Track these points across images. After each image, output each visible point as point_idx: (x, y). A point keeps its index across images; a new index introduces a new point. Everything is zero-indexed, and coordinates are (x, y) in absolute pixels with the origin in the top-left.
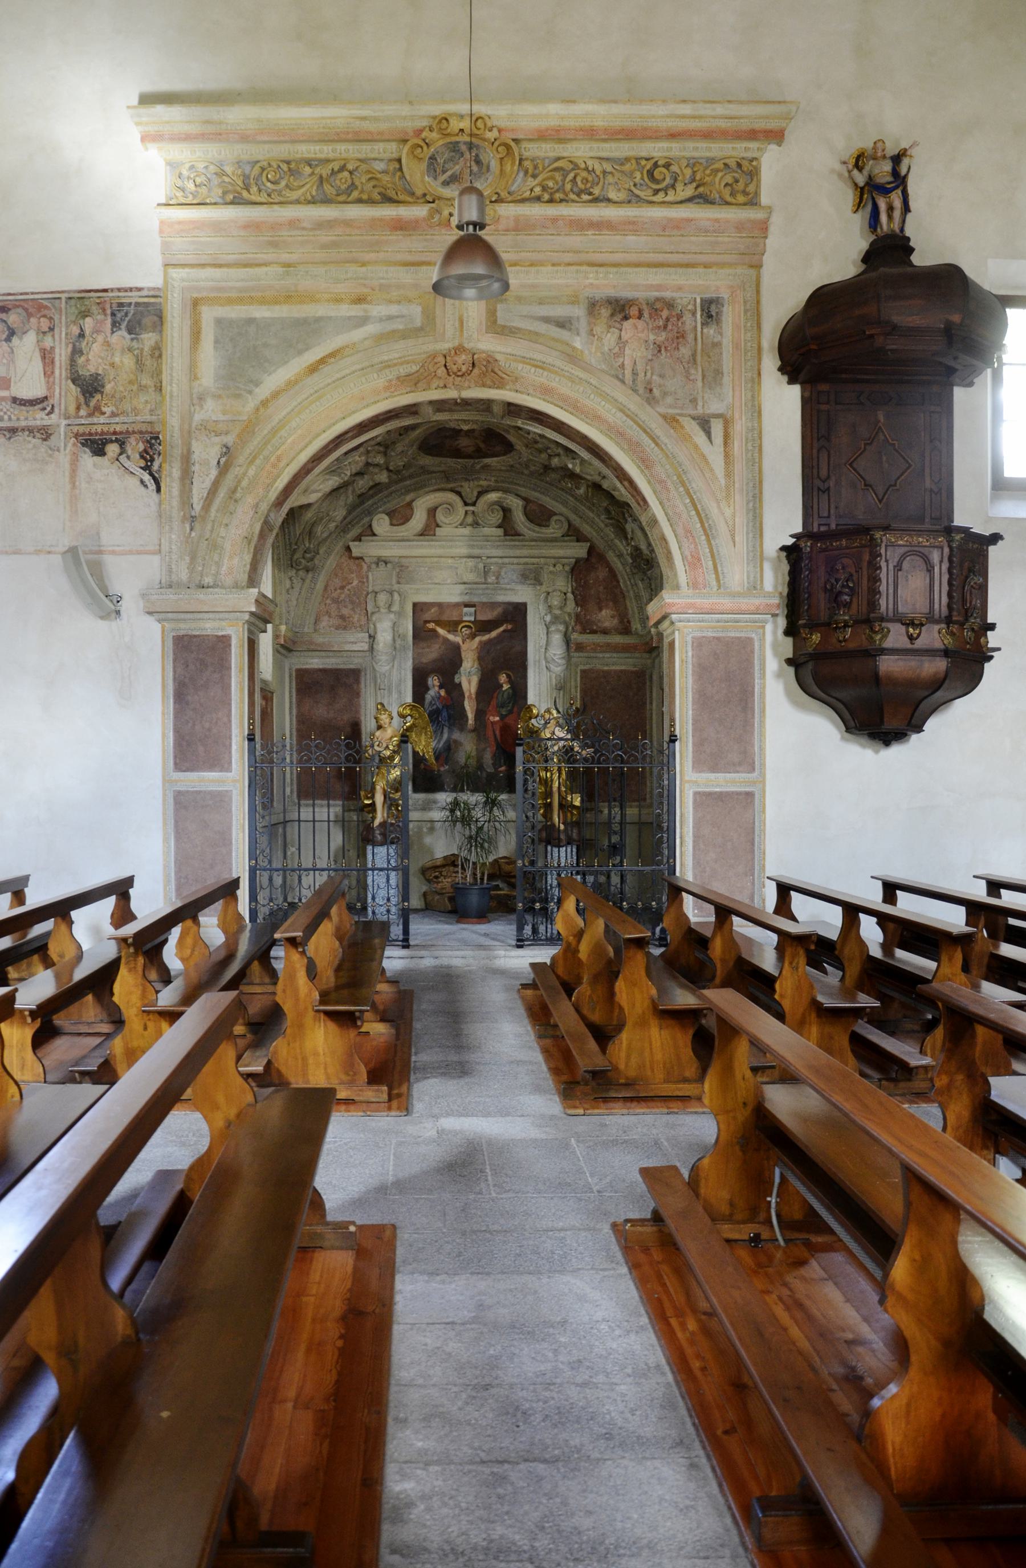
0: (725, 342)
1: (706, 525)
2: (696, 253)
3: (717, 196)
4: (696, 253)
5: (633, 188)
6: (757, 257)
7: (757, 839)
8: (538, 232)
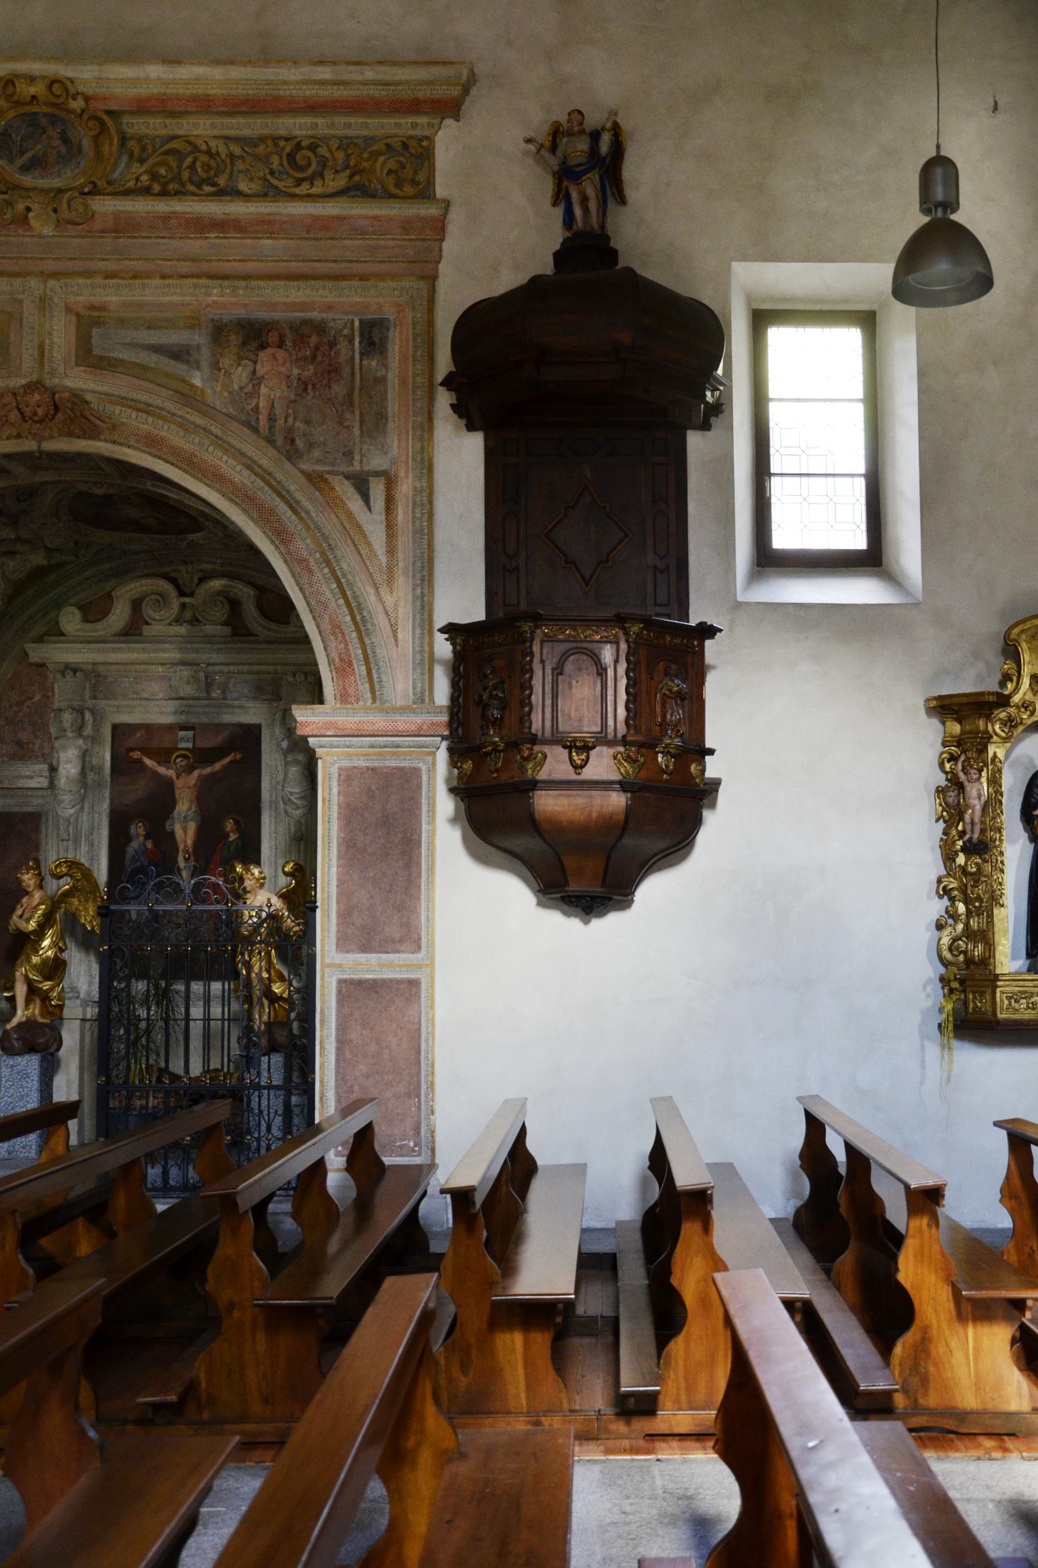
0: (390, 375)
1: (358, 618)
2: (350, 261)
3: (379, 186)
4: (350, 261)
5: (269, 177)
6: (432, 265)
7: (423, 1046)
8: (143, 234)
